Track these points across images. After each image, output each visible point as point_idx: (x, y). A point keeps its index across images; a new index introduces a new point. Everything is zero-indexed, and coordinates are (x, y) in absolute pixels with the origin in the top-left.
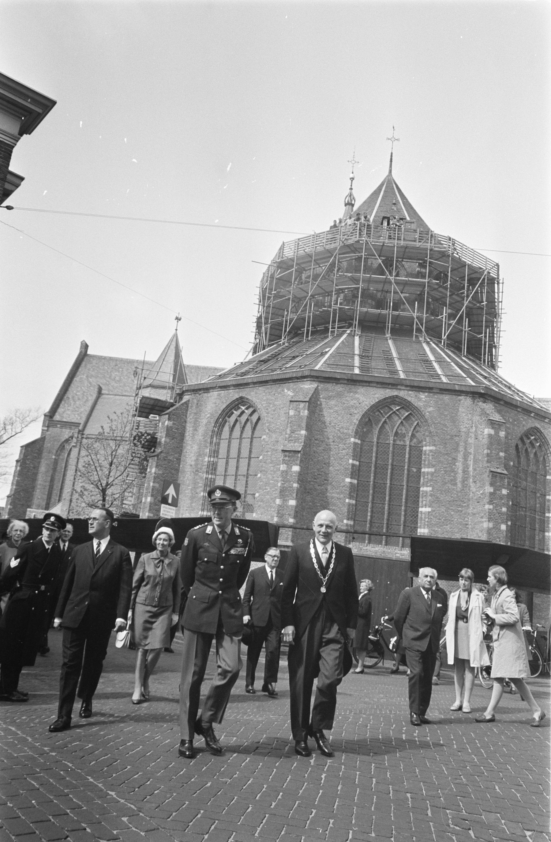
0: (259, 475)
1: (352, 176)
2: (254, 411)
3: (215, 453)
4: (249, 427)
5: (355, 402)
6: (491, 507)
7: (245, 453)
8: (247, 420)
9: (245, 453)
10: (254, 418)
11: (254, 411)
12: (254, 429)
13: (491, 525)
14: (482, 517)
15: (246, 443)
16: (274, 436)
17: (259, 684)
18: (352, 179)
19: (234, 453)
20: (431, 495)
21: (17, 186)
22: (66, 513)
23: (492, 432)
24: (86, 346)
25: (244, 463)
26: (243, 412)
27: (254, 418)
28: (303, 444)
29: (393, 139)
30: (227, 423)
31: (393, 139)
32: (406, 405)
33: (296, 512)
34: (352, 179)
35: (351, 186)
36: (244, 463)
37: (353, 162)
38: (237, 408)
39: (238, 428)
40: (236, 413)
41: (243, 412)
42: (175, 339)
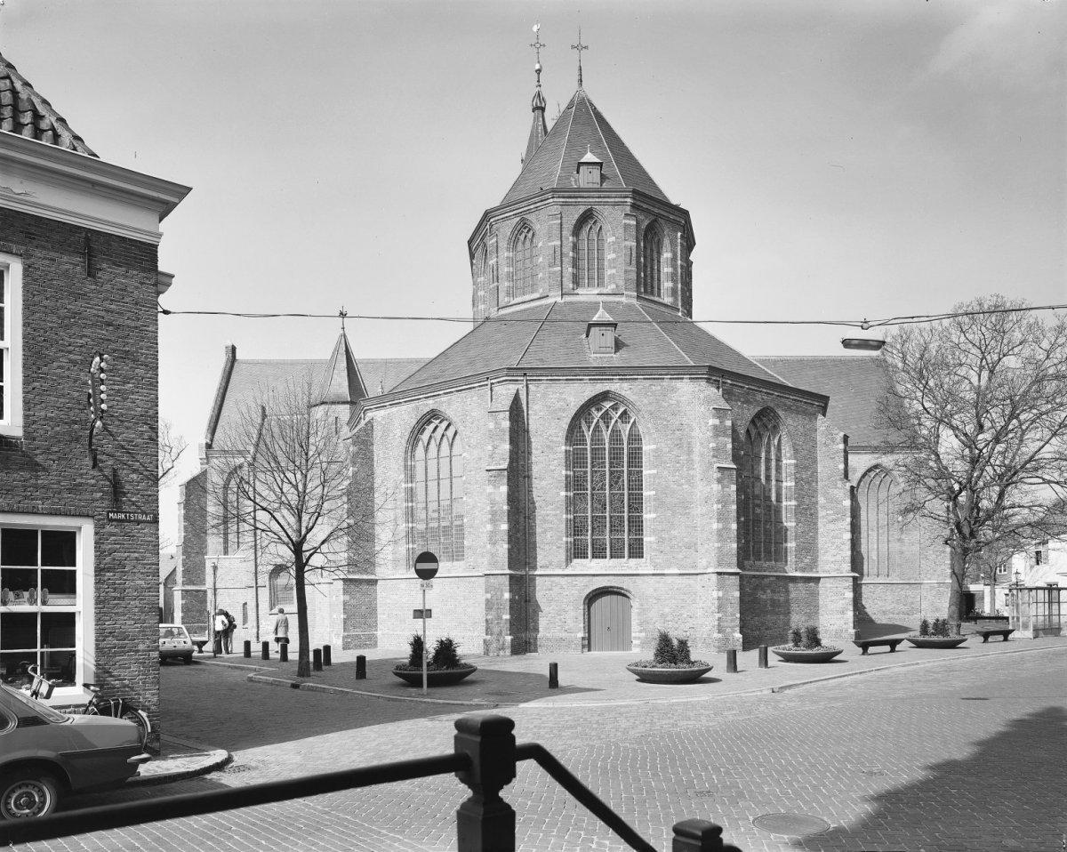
0: (465, 499)
1: (537, 67)
2: (449, 425)
3: (411, 478)
4: (445, 444)
6: (720, 506)
7: (445, 473)
8: (443, 435)
9: (445, 473)
10: (450, 433)
11: (449, 425)
12: (451, 445)
13: (720, 526)
14: (711, 518)
15: (445, 463)
16: (475, 452)
17: (642, 290)
18: (539, 71)
19: (432, 473)
20: (655, 500)
21: (169, 285)
22: (249, 563)
23: (717, 422)
24: (234, 349)
25: (445, 484)
26: (436, 427)
27: (450, 433)
28: (508, 460)
29: (579, 47)
30: (420, 442)
31: (579, 47)
32: (618, 399)
33: (510, 537)
34: (539, 71)
35: (539, 81)
36: (445, 484)
37: (538, 45)
38: (429, 422)
39: (433, 446)
40: (430, 428)
41: (436, 427)
42: (343, 339)
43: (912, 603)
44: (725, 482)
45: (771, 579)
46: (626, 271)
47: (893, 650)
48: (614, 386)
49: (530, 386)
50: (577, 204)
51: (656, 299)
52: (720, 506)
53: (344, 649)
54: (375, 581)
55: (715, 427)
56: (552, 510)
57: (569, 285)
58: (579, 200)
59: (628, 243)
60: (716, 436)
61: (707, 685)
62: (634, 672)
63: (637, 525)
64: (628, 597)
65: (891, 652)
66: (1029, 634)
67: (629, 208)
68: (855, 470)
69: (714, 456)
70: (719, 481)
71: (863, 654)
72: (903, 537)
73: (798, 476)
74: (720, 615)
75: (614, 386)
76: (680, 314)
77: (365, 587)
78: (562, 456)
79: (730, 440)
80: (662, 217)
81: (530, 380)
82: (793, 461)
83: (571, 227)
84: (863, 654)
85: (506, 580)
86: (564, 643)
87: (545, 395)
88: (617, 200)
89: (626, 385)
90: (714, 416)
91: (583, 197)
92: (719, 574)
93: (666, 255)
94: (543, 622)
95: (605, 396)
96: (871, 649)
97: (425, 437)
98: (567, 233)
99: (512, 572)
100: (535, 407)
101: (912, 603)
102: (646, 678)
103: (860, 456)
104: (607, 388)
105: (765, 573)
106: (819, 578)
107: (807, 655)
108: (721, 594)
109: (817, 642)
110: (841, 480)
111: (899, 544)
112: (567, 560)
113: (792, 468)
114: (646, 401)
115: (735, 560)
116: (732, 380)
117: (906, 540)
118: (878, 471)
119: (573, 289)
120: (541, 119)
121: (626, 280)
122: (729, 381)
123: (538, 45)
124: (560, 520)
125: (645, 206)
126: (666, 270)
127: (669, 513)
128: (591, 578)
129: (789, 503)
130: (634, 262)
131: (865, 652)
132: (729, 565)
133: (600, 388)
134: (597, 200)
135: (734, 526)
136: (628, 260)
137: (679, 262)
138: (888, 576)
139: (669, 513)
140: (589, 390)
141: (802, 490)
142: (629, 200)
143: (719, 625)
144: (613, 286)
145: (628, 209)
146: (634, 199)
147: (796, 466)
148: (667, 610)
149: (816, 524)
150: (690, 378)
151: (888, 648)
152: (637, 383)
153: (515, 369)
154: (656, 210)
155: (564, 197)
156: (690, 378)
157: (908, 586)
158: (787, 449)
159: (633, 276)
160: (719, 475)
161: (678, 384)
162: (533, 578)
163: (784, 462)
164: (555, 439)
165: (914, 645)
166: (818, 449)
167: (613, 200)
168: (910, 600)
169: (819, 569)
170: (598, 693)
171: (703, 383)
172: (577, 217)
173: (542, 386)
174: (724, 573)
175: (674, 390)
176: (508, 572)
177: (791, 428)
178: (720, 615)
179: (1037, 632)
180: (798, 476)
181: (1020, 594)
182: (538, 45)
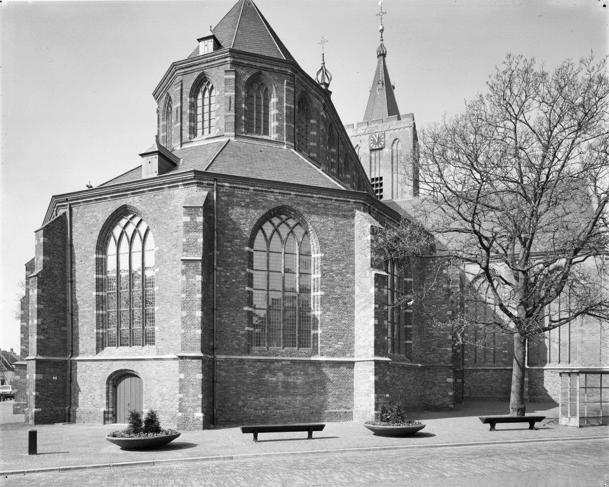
1: (381, 28)
5: (94, 220)
18: (382, 31)
23: (188, 219)
34: (382, 31)
35: (382, 37)
44: (190, 273)
45: (284, 363)
46: (226, 117)
47: (310, 437)
48: (131, 201)
49: (73, 209)
50: (193, 71)
51: (265, 137)
52: (184, 296)
53: (14, 413)
54: (351, 365)
55: (186, 224)
56: (88, 307)
57: (186, 135)
58: (194, 68)
59: (228, 94)
60: (187, 231)
61: (425, 439)
62: (372, 429)
63: (147, 317)
64: (137, 376)
65: (308, 438)
66: (575, 422)
67: (229, 65)
69: (184, 251)
70: (184, 272)
71: (491, 430)
72: (584, 328)
73: (325, 268)
74: (181, 396)
75: (131, 201)
76: (285, 147)
77: (344, 369)
78: (94, 262)
79: (201, 235)
80: (266, 69)
81: (73, 204)
82: (320, 255)
83: (189, 90)
84: (491, 430)
85: (372, 367)
86: (92, 416)
87: (83, 215)
88: (220, 61)
89: (137, 198)
90: (185, 214)
91: (196, 65)
92: (181, 358)
93: (274, 100)
94: (81, 397)
95: (123, 211)
96: (498, 426)
97: (117, 231)
98: (186, 96)
99: (41, 358)
100: (77, 225)
102: (129, 446)
104: (124, 203)
105: (278, 358)
106: (353, 363)
107: (387, 430)
108: (182, 376)
109: (157, 430)
110: (369, 269)
111: (580, 335)
112: (97, 347)
113: (319, 261)
114: (151, 210)
115: (199, 344)
116: (230, 183)
117: (587, 331)
119: (190, 138)
120: (382, 62)
121: (226, 123)
122: (227, 184)
124: (93, 316)
125: (246, 62)
126: (273, 112)
127: (168, 305)
128: (112, 362)
129: (316, 293)
130: (233, 108)
131: (493, 428)
132: (193, 350)
133: (120, 203)
134: (206, 65)
135: (199, 314)
136: (228, 108)
137: (285, 104)
138: (569, 362)
139: (168, 305)
140: (111, 206)
141: (331, 281)
142: (228, 59)
143: (180, 405)
144: (218, 130)
145: (228, 67)
146: (234, 57)
147: (323, 259)
148: (165, 390)
149: (352, 312)
150: (184, 185)
151: (527, 425)
152: (144, 195)
154: (258, 65)
155: (183, 68)
156: (184, 185)
158: (315, 244)
159: (232, 119)
160: (184, 267)
161: (175, 191)
162: (73, 364)
163: (313, 256)
164: (89, 249)
165: (421, 431)
166: (355, 243)
167: (217, 62)
169: (355, 354)
170: (184, 451)
171: (195, 188)
172: (192, 81)
173: (81, 207)
174: (186, 357)
175: (172, 197)
176: (373, 358)
177: (316, 225)
178: (181, 396)
179: (586, 422)
180: (325, 268)
182: (381, 14)
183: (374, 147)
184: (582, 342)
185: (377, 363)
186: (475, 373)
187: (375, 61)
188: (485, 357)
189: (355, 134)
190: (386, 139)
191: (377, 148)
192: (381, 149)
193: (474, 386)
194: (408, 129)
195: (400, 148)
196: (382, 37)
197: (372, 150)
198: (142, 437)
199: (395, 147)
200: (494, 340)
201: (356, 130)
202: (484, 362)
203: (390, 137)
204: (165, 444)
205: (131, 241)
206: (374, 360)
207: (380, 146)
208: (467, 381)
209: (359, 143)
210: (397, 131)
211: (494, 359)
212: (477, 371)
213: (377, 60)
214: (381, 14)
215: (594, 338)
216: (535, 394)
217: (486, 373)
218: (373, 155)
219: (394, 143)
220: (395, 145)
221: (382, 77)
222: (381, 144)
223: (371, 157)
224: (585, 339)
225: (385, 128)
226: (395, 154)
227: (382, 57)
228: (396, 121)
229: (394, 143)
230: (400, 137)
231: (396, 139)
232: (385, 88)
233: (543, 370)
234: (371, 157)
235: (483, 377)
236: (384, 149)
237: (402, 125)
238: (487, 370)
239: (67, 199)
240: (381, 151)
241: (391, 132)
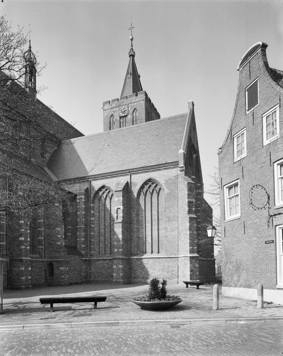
1: (131, 37)
11: (109, 191)
18: (132, 39)
26: (150, 186)
27: (110, 195)
34: (132, 39)
35: (132, 44)
41: (150, 186)
43: (172, 271)
68: (136, 184)
97: (145, 190)
101: (172, 271)
102: (144, 307)
103: (139, 175)
117: (169, 228)
118: (104, 190)
123: (132, 28)
153: (165, 163)
157: (169, 260)
168: (171, 269)
176: (189, 255)
181: (274, 218)
182: (131, 28)
183: (122, 115)
184: (166, 237)
185: (191, 258)
186: (97, 263)
187: (128, 59)
188: (105, 250)
189: (110, 107)
190: (129, 109)
191: (124, 115)
192: (126, 116)
193: (97, 272)
194: (142, 102)
195: (137, 115)
196: (132, 44)
197: (121, 117)
198: (157, 301)
199: (134, 114)
200: (111, 237)
201: (111, 105)
202: (105, 254)
203: (131, 108)
204: (173, 306)
205: (145, 195)
206: (190, 256)
207: (126, 114)
208: (92, 268)
209: (113, 113)
210: (135, 103)
211: (111, 251)
212: (99, 260)
213: (129, 58)
214: (131, 28)
215: (174, 233)
216: (135, 278)
217: (104, 262)
218: (121, 121)
219: (134, 111)
220: (135, 113)
221: (131, 71)
222: (126, 113)
223: (120, 122)
224: (168, 234)
225: (128, 102)
226: (134, 119)
227: (131, 57)
228: (135, 97)
229: (134, 111)
230: (137, 107)
231: (135, 109)
232: (132, 77)
233: (141, 259)
234: (120, 122)
235: (102, 265)
236: (128, 116)
237: (138, 100)
238: (105, 260)
239: (129, 171)
240: (126, 118)
241: (133, 104)
